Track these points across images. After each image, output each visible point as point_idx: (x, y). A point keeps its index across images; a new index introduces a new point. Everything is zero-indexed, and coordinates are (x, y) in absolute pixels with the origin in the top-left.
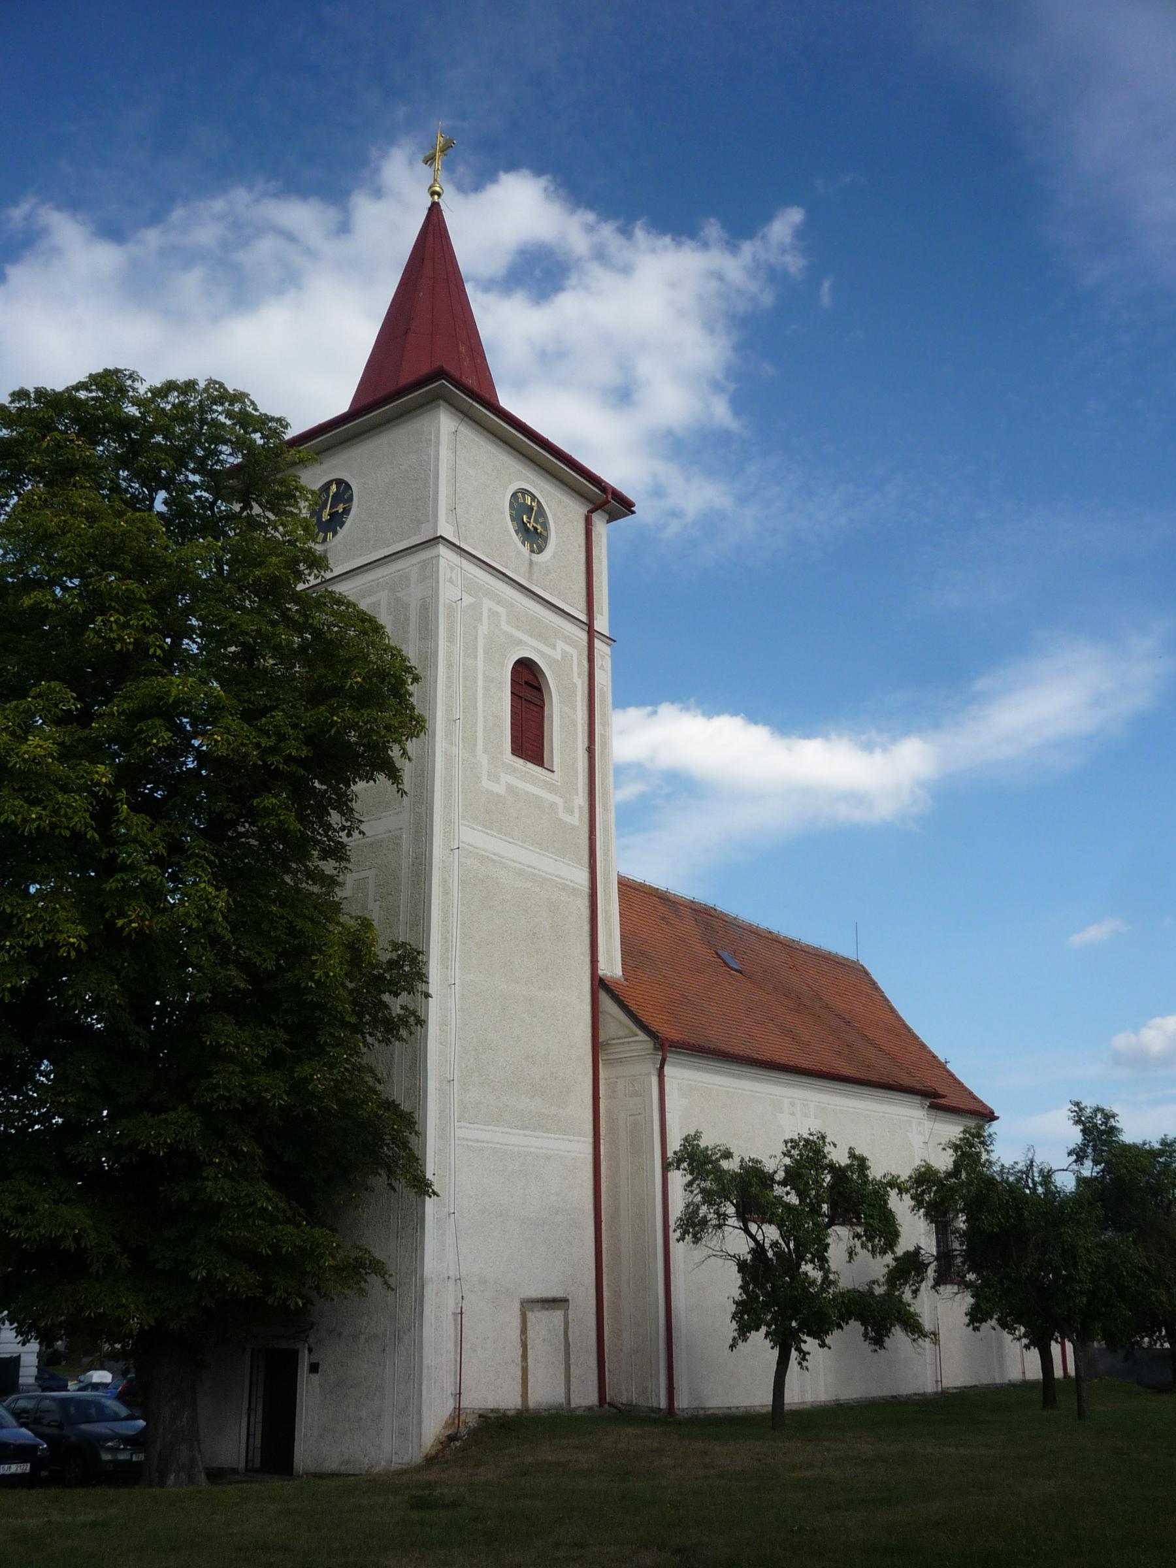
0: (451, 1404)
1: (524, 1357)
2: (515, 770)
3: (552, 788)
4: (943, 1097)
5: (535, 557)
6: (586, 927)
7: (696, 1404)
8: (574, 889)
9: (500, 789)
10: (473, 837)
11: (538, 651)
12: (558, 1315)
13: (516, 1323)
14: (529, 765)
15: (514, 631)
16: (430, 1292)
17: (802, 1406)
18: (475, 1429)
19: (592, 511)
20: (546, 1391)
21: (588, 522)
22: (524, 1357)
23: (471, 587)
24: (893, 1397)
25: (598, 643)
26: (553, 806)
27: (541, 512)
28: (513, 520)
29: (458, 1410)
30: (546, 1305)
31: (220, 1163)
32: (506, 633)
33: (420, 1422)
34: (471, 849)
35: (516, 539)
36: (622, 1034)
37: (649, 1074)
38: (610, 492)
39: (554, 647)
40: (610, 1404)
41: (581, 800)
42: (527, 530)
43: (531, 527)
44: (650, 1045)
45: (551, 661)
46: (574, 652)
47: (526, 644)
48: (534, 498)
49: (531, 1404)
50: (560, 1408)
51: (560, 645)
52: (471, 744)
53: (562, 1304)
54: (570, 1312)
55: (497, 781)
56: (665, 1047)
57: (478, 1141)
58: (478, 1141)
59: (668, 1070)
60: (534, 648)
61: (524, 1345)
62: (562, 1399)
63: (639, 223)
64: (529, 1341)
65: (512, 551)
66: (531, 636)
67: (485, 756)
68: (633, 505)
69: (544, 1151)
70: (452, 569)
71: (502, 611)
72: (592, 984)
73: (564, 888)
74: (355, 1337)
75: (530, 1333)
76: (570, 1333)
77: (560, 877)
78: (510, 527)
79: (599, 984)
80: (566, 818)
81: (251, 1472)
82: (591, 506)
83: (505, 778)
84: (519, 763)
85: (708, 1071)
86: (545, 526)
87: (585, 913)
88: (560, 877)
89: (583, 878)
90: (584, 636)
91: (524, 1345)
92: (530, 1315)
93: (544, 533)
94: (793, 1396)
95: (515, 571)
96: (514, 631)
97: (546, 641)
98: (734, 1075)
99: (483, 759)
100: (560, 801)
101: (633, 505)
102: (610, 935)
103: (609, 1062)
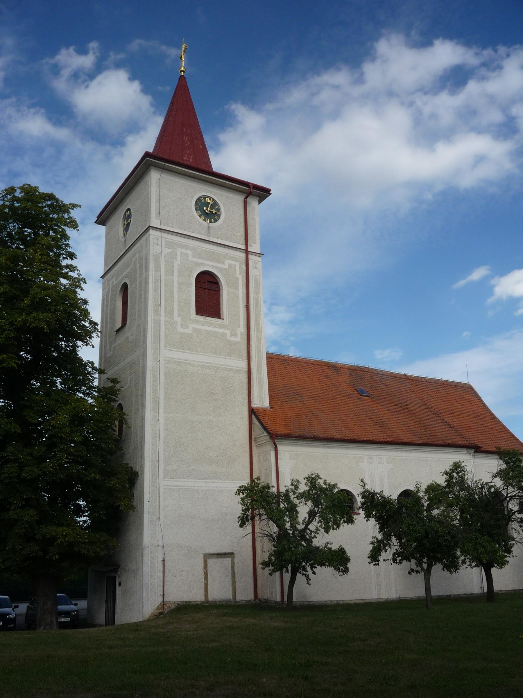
0: (161, 599)
1: (206, 578)
2: (198, 321)
3: (222, 327)
4: (482, 447)
5: (211, 225)
6: (246, 386)
7: (302, 599)
8: (237, 370)
9: (189, 331)
10: (168, 353)
11: (212, 266)
12: (228, 561)
13: (202, 564)
14: (207, 318)
15: (198, 260)
16: (146, 552)
17: (378, 600)
18: (173, 610)
19: (246, 198)
20: (220, 592)
21: (245, 203)
22: (206, 578)
23: (169, 245)
24: (447, 596)
25: (250, 256)
26: (223, 335)
27: (215, 204)
28: (197, 210)
29: (164, 603)
30: (220, 556)
31: (16, 503)
32: (192, 261)
33: (143, 607)
34: (171, 359)
35: (201, 220)
36: (260, 433)
37: (270, 450)
38: (252, 187)
39: (223, 263)
40: (259, 600)
41: (242, 329)
42: (207, 214)
43: (209, 211)
44: (268, 437)
45: (221, 270)
46: (237, 264)
47: (205, 264)
48: (210, 198)
49: (210, 599)
50: (229, 601)
51: (227, 262)
52: (170, 313)
53: (231, 555)
54: (235, 559)
55: (187, 327)
56: (275, 437)
57: (176, 486)
58: (176, 486)
59: (279, 448)
60: (210, 266)
61: (206, 574)
62: (203, 599)
63: (74, 47)
64: (208, 572)
65: (199, 225)
66: (208, 260)
67: (180, 318)
68: (270, 190)
69: (219, 488)
70: (158, 239)
71: (190, 252)
72: (249, 412)
73: (231, 370)
74: (129, 571)
75: (209, 569)
76: (236, 568)
77: (228, 366)
78: (196, 214)
79: (252, 412)
80: (233, 339)
81: (107, 624)
82: (246, 195)
83: (191, 326)
84: (201, 318)
85: (297, 445)
86: (219, 210)
87: (246, 380)
88: (228, 366)
89: (244, 364)
90: (243, 255)
91: (206, 574)
92: (209, 561)
93: (218, 213)
94: (497, 588)
95: (199, 233)
96: (198, 260)
97: (218, 261)
98: (328, 447)
99: (178, 319)
100: (228, 332)
101: (270, 190)
102: (261, 388)
103: (258, 446)
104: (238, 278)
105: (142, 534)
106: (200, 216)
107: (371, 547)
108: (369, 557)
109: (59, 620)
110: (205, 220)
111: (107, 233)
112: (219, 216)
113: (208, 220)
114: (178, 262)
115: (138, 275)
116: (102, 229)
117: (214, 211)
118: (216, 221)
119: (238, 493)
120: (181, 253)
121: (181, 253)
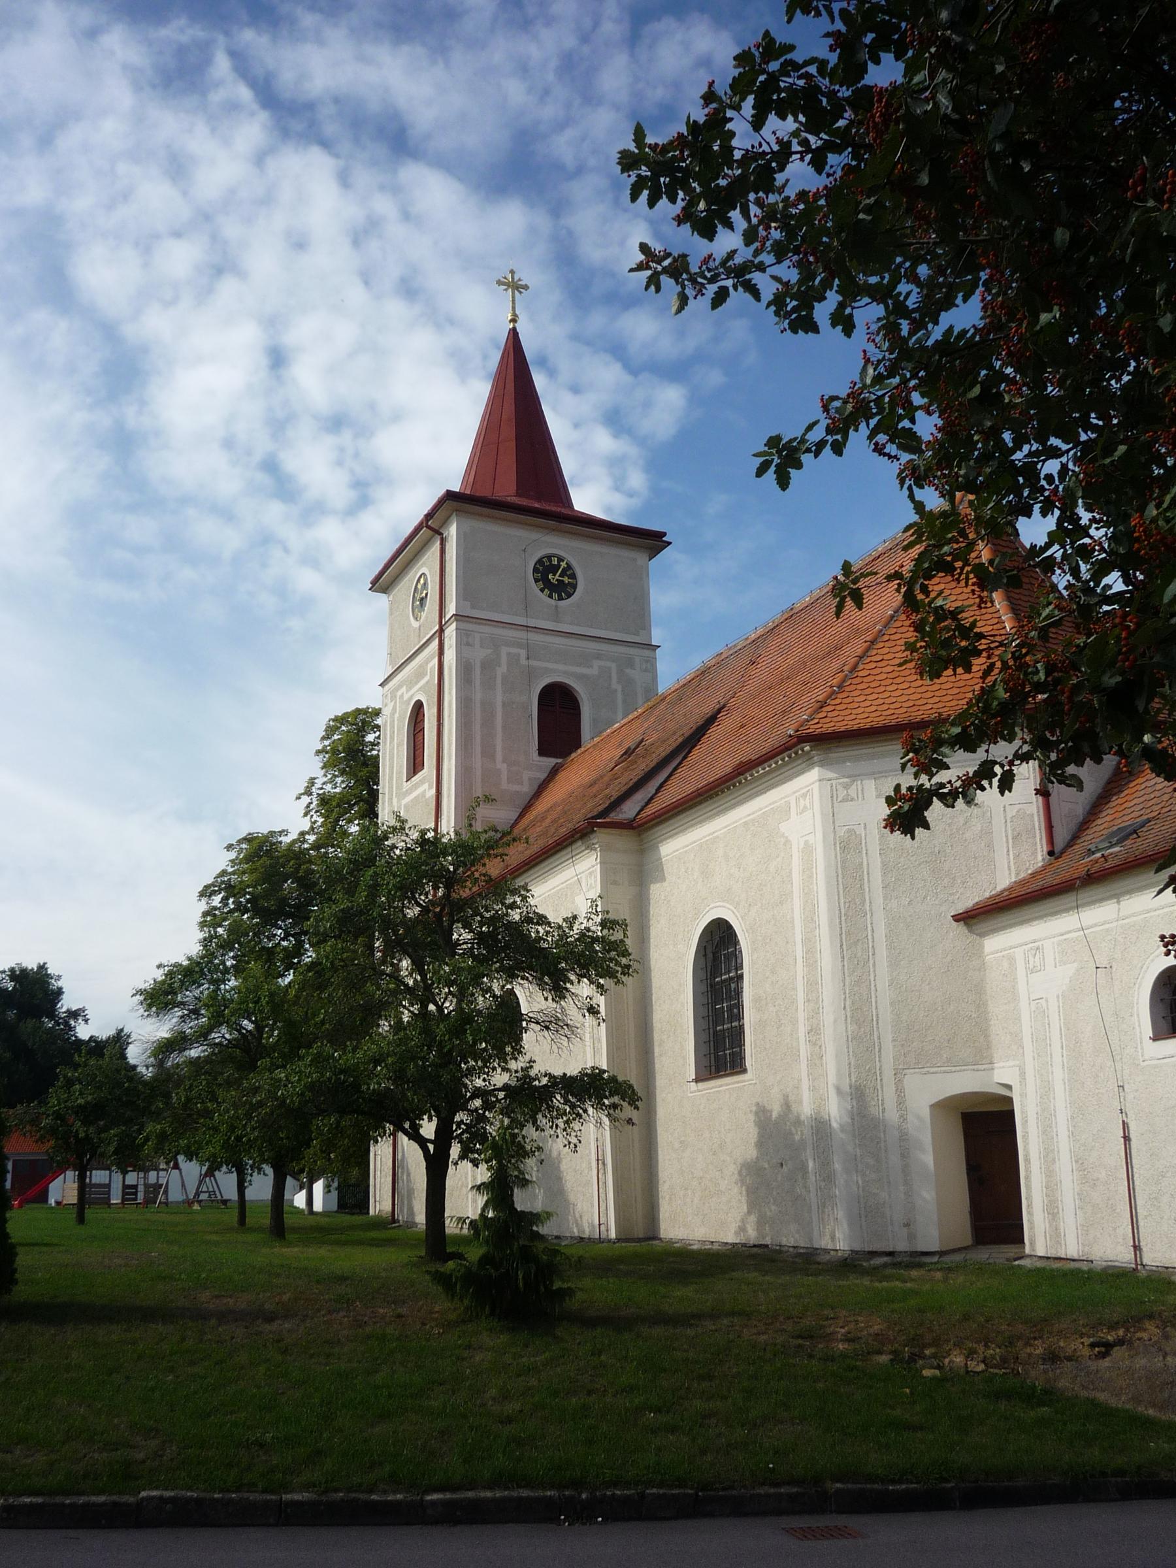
35: (543, 597)
45: (581, 677)
86: (573, 576)
104: (618, 682)
105: (802, 772)
106: (542, 590)
107: (159, 975)
108: (189, 959)
109: (1011, 445)
110: (550, 596)
111: (392, 603)
112: (574, 587)
113: (555, 596)
114: (501, 670)
115: (525, 1493)
116: (382, 600)
117: (566, 580)
118: (569, 596)
119: (207, 892)
120: (509, 654)
121: (509, 654)
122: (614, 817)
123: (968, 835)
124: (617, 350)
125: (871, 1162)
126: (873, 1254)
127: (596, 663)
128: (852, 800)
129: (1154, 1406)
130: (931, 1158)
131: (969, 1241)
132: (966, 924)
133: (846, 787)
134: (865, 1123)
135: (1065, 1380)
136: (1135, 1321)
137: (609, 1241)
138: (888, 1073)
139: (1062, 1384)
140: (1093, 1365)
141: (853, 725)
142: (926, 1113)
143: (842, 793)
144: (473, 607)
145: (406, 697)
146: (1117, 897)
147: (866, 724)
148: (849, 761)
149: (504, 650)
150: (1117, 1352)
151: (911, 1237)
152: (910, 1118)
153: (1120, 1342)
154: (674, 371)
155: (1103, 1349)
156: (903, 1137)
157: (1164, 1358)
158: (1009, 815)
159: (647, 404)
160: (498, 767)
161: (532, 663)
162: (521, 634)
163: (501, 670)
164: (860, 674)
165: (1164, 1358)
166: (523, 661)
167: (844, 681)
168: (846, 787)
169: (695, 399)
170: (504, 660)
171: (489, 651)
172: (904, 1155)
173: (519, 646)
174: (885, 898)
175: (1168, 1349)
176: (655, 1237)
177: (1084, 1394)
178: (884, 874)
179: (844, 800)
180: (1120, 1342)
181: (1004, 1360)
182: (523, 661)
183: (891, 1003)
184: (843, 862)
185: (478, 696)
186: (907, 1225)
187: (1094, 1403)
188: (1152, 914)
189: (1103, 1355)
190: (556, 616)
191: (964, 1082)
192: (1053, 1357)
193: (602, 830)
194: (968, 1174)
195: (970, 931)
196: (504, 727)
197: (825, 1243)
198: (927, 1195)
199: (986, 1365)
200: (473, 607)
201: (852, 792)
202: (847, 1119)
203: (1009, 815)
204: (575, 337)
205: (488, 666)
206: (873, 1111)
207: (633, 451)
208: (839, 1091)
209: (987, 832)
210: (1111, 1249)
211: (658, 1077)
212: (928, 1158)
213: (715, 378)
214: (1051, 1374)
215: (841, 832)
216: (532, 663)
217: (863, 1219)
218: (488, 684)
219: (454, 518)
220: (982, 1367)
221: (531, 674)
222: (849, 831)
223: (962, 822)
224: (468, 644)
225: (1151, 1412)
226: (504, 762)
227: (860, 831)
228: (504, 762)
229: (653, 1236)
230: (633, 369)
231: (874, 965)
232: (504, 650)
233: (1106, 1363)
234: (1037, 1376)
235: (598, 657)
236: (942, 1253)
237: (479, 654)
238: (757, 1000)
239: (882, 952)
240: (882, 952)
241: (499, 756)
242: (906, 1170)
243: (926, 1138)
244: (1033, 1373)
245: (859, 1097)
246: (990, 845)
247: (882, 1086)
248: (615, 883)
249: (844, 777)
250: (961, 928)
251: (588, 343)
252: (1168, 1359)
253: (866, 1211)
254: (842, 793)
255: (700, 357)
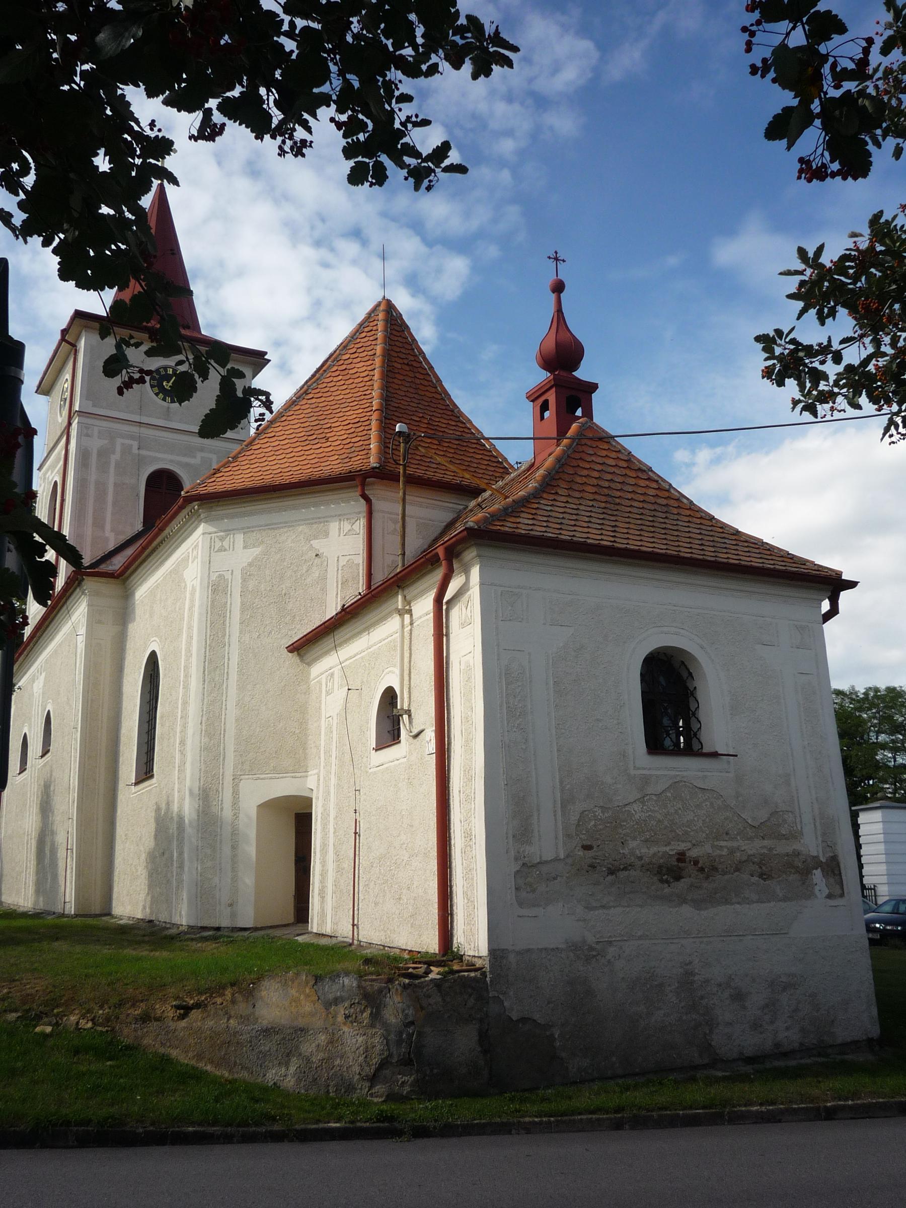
35: (158, 400)
45: (187, 465)
114: (115, 457)
120: (123, 444)
122: (103, 568)
123: (308, 580)
124: (417, 226)
125: (209, 851)
126: (204, 928)
127: (199, 455)
128: (225, 550)
129: (212, 1062)
130: (254, 852)
131: (291, 919)
132: (299, 655)
133: (222, 539)
134: (208, 820)
135: (151, 1039)
136: (220, 989)
137: (68, 916)
138: (228, 779)
139: (146, 1041)
140: (172, 1025)
141: (238, 485)
142: (253, 812)
143: (218, 544)
144: (94, 406)
145: (50, 478)
146: (367, 629)
147: (248, 484)
148: (227, 518)
149: (119, 441)
150: (195, 1014)
151: (233, 915)
152: (241, 816)
153: (197, 1006)
154: (460, 245)
155: (182, 1011)
156: (235, 832)
157: (228, 1020)
158: (341, 564)
159: (439, 271)
160: (107, 535)
161: (143, 452)
162: (135, 429)
163: (115, 457)
164: (254, 447)
165: (228, 1020)
166: (135, 451)
167: (240, 453)
168: (222, 539)
169: (476, 269)
170: (118, 448)
171: (106, 442)
172: (234, 847)
173: (132, 438)
174: (241, 632)
175: (232, 1013)
176: (109, 914)
177: (162, 1050)
178: (242, 612)
179: (220, 550)
180: (197, 1006)
181: (108, 1020)
182: (135, 451)
183: (236, 720)
184: (213, 602)
185: (93, 477)
186: (231, 905)
187: (166, 1060)
188: (383, 642)
189: (182, 1017)
190: (167, 414)
191: (284, 787)
192: (145, 1018)
193: (90, 578)
194: (296, 864)
195: (302, 660)
196: (115, 503)
197: (176, 920)
198: (248, 880)
199: (94, 1023)
200: (94, 406)
201: (226, 544)
202: (195, 816)
203: (341, 564)
204: (384, 214)
205: (104, 454)
206: (214, 810)
207: (427, 308)
208: (191, 793)
209: (323, 578)
210: (344, 931)
211: (120, 782)
212: (250, 850)
213: (493, 252)
214: (139, 1033)
215: (214, 577)
216: (143, 452)
217: (199, 899)
218: (103, 467)
219: (84, 333)
220: (90, 1025)
221: (141, 461)
222: (220, 576)
223: (305, 570)
224: (87, 435)
225: (209, 1068)
226: (112, 531)
227: (228, 576)
228: (112, 531)
229: (107, 913)
230: (429, 242)
231: (227, 688)
232: (119, 441)
233: (183, 1023)
234: (127, 1034)
235: (202, 450)
236: (256, 929)
237: (95, 444)
238: (162, 717)
239: (234, 676)
240: (234, 676)
241: (108, 527)
242: (234, 857)
243: (252, 834)
244: (126, 1031)
245: (206, 797)
246: (324, 590)
247: (223, 788)
248: (100, 622)
249: (221, 531)
250: (293, 658)
251: (394, 219)
252: (231, 1021)
253: (203, 894)
254: (218, 544)
255: (481, 234)
